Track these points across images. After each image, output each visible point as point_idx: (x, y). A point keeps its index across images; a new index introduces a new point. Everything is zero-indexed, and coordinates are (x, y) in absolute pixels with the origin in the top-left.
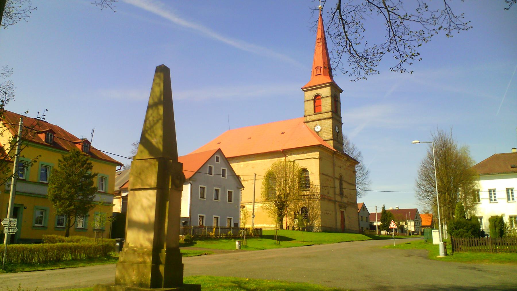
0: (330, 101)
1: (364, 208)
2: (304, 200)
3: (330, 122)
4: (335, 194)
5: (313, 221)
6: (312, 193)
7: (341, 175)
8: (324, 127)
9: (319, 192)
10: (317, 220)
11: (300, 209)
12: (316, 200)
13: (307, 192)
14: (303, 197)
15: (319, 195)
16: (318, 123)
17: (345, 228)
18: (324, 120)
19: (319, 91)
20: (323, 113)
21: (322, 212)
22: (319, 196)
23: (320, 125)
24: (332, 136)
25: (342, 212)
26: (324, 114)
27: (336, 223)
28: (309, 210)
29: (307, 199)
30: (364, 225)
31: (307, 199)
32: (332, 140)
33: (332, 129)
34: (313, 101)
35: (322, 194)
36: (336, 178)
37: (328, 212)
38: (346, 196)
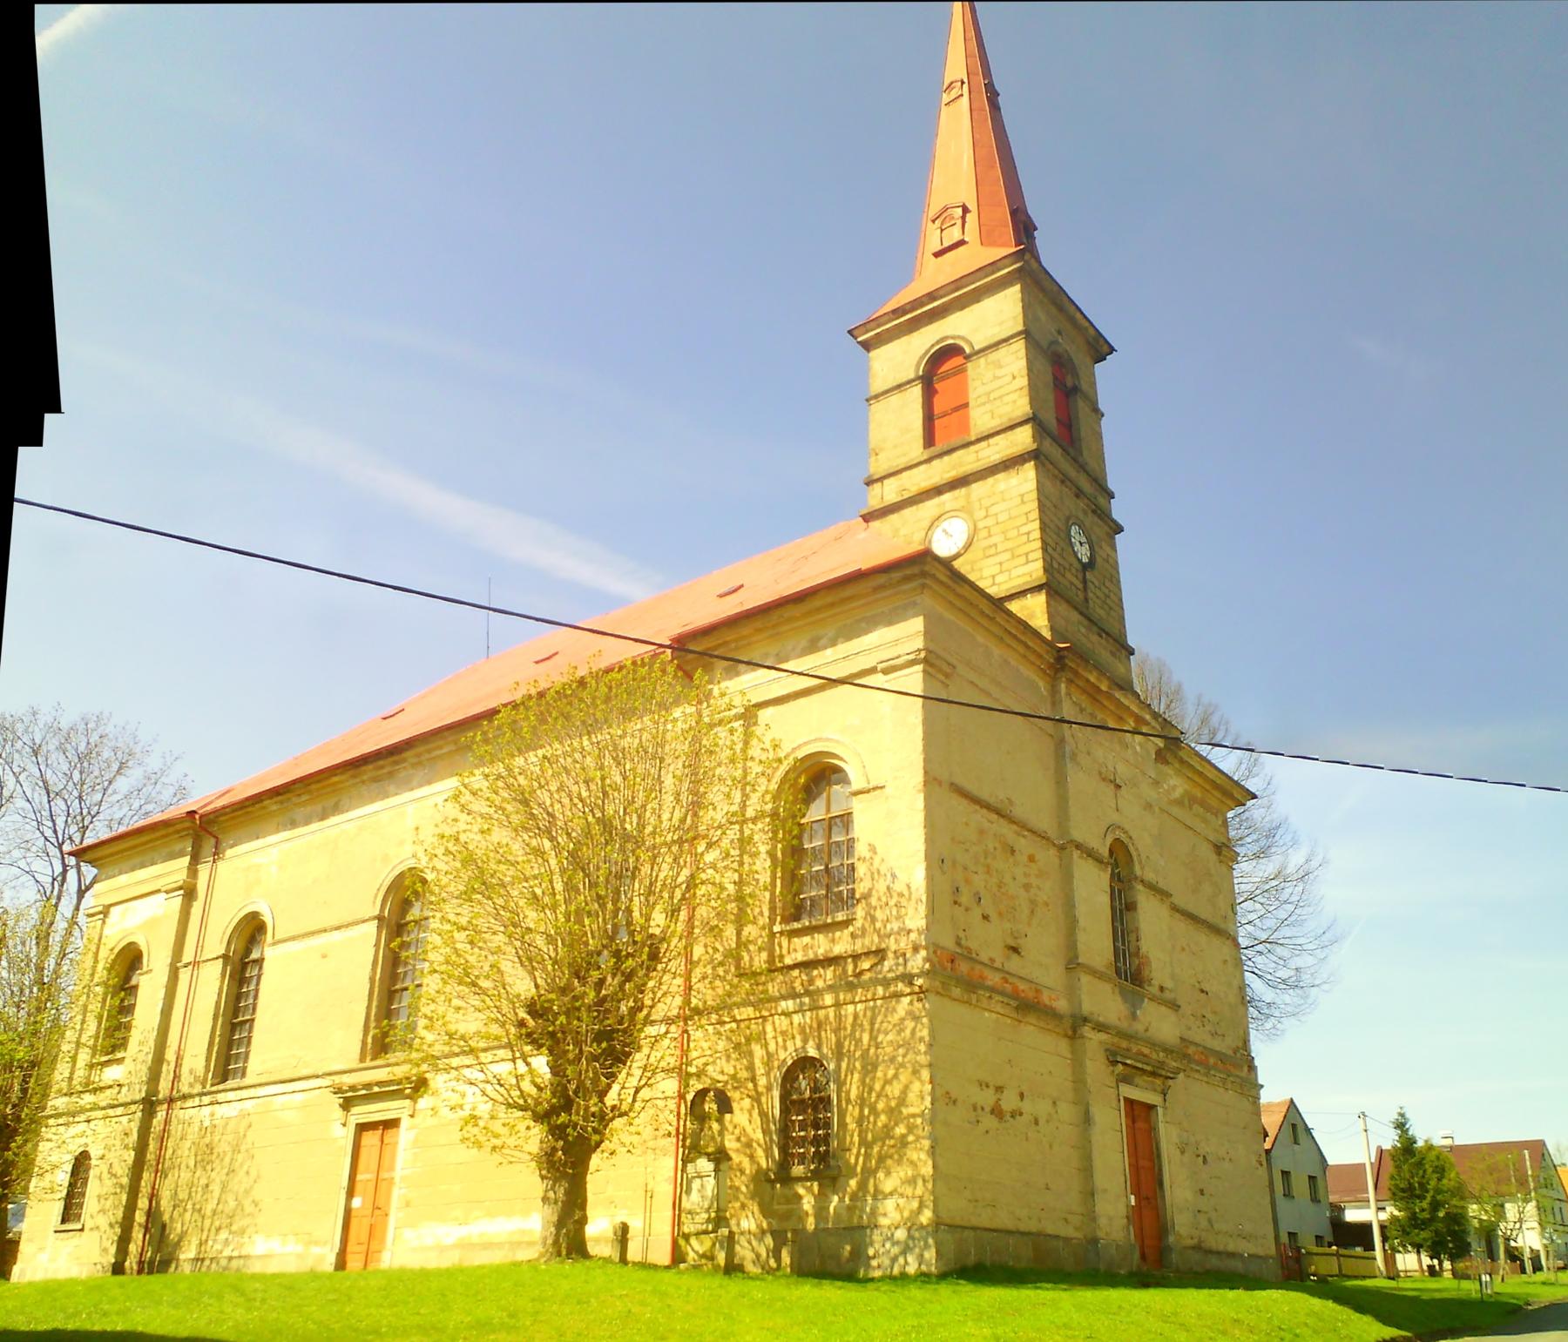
0: (1023, 363)
1: (1294, 1126)
2: (806, 1000)
3: (1026, 480)
4: (1073, 964)
5: (869, 1173)
6: (867, 941)
7: (1118, 834)
8: (990, 522)
9: (922, 923)
10: (899, 1162)
11: (777, 1075)
12: (898, 996)
13: (833, 941)
14: (798, 978)
15: (923, 953)
16: (948, 507)
17: (1171, 1239)
18: (991, 480)
19: (956, 326)
20: (979, 440)
21: (943, 1098)
22: (917, 963)
23: (966, 510)
24: (1039, 564)
25: (1138, 1114)
26: (984, 444)
27: (1090, 1194)
28: (840, 1085)
29: (830, 988)
30: (1306, 1221)
31: (830, 988)
32: (1036, 589)
33: (1037, 524)
34: (916, 391)
35: (949, 943)
36: (1078, 846)
37: (1009, 1102)
38: (1167, 995)
